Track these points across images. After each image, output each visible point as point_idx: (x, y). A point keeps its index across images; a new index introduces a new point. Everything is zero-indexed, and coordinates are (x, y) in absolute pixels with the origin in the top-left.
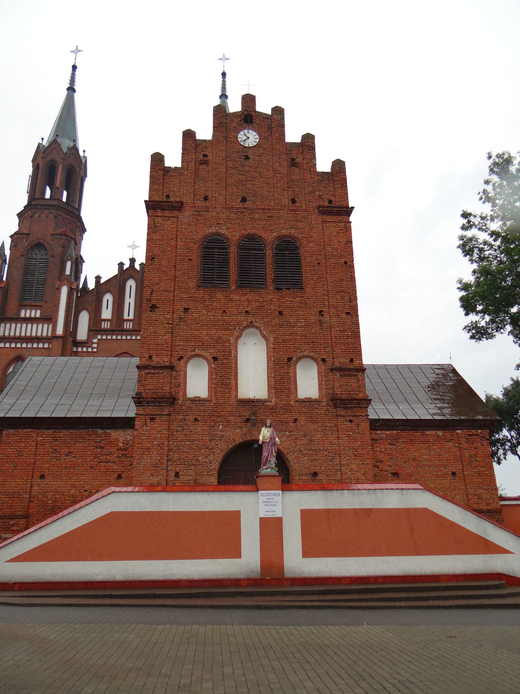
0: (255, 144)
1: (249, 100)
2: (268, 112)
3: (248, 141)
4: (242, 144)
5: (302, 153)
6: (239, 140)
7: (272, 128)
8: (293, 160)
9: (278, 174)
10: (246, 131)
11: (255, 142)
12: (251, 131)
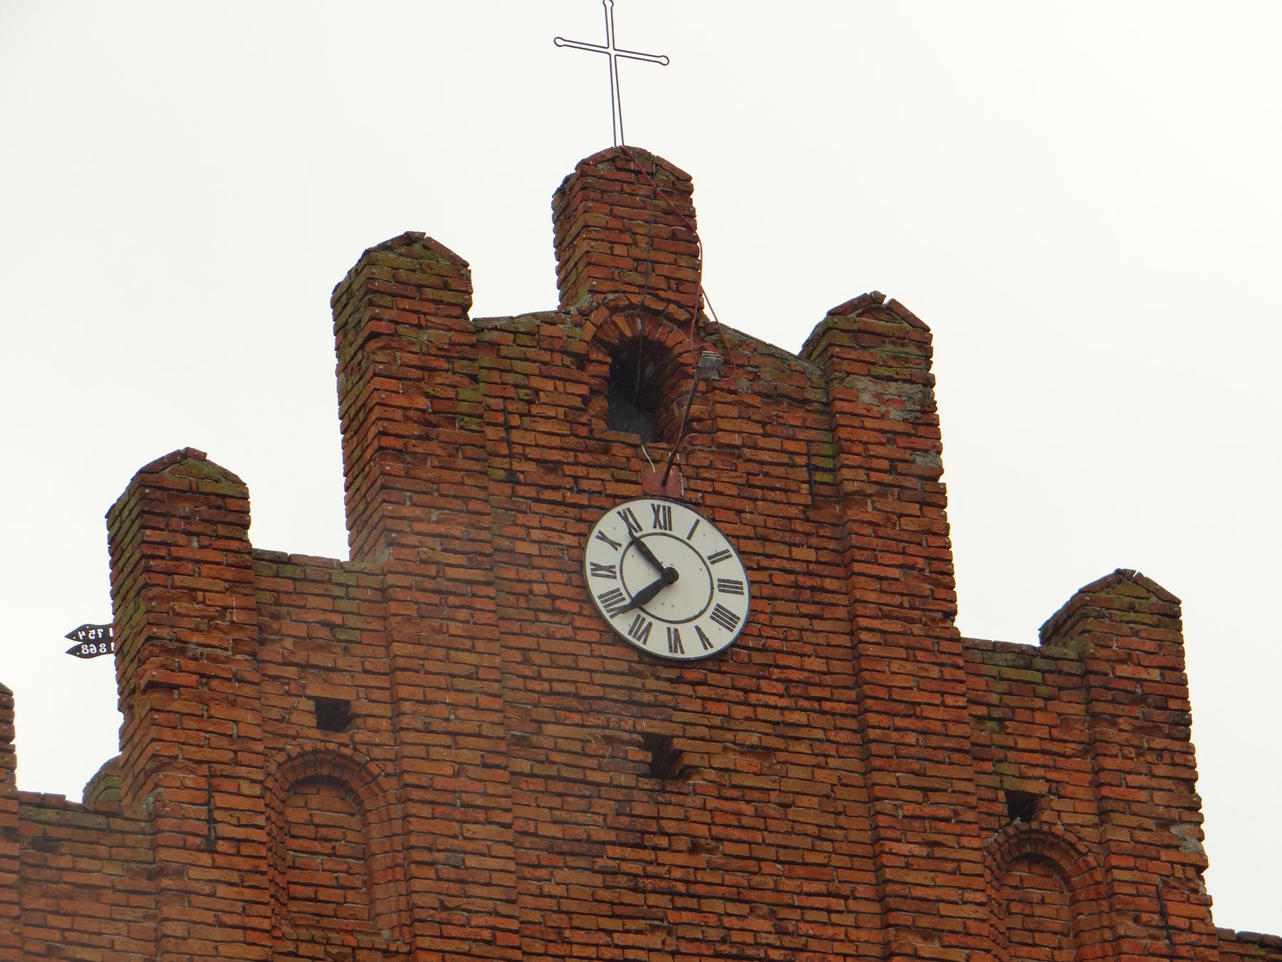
0: (722, 638)
1: (627, 211)
2: (786, 325)
3: (668, 606)
4: (622, 625)
5: (1091, 748)
6: (598, 586)
7: (847, 499)
8: (1023, 805)
9: (928, 934)
10: (643, 510)
11: (724, 617)
12: (683, 517)
